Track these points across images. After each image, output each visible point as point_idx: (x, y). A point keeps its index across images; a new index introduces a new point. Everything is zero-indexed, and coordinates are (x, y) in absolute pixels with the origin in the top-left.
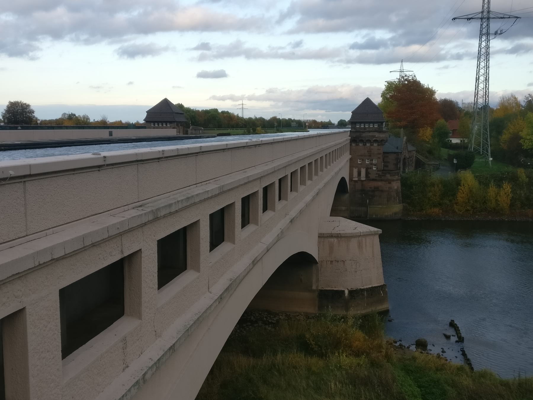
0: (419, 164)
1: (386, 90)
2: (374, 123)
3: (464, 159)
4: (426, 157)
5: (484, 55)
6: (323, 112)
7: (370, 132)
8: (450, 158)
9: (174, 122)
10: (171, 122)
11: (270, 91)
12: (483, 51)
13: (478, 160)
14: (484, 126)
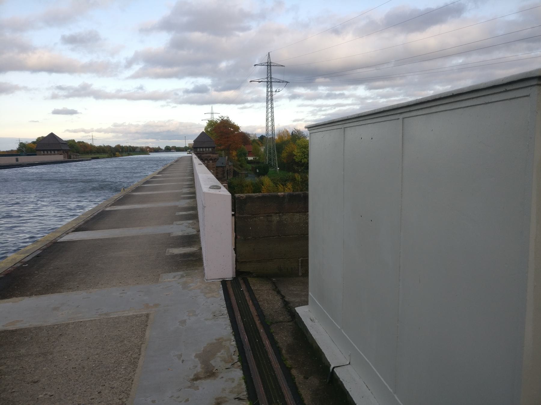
0: (235, 174)
1: (208, 126)
2: (209, 148)
3: (262, 169)
4: (239, 169)
5: (270, 99)
6: (154, 140)
7: (207, 153)
8: (254, 170)
9: (61, 150)
10: (58, 150)
11: (115, 125)
12: (269, 98)
13: (271, 170)
14: (270, 151)
